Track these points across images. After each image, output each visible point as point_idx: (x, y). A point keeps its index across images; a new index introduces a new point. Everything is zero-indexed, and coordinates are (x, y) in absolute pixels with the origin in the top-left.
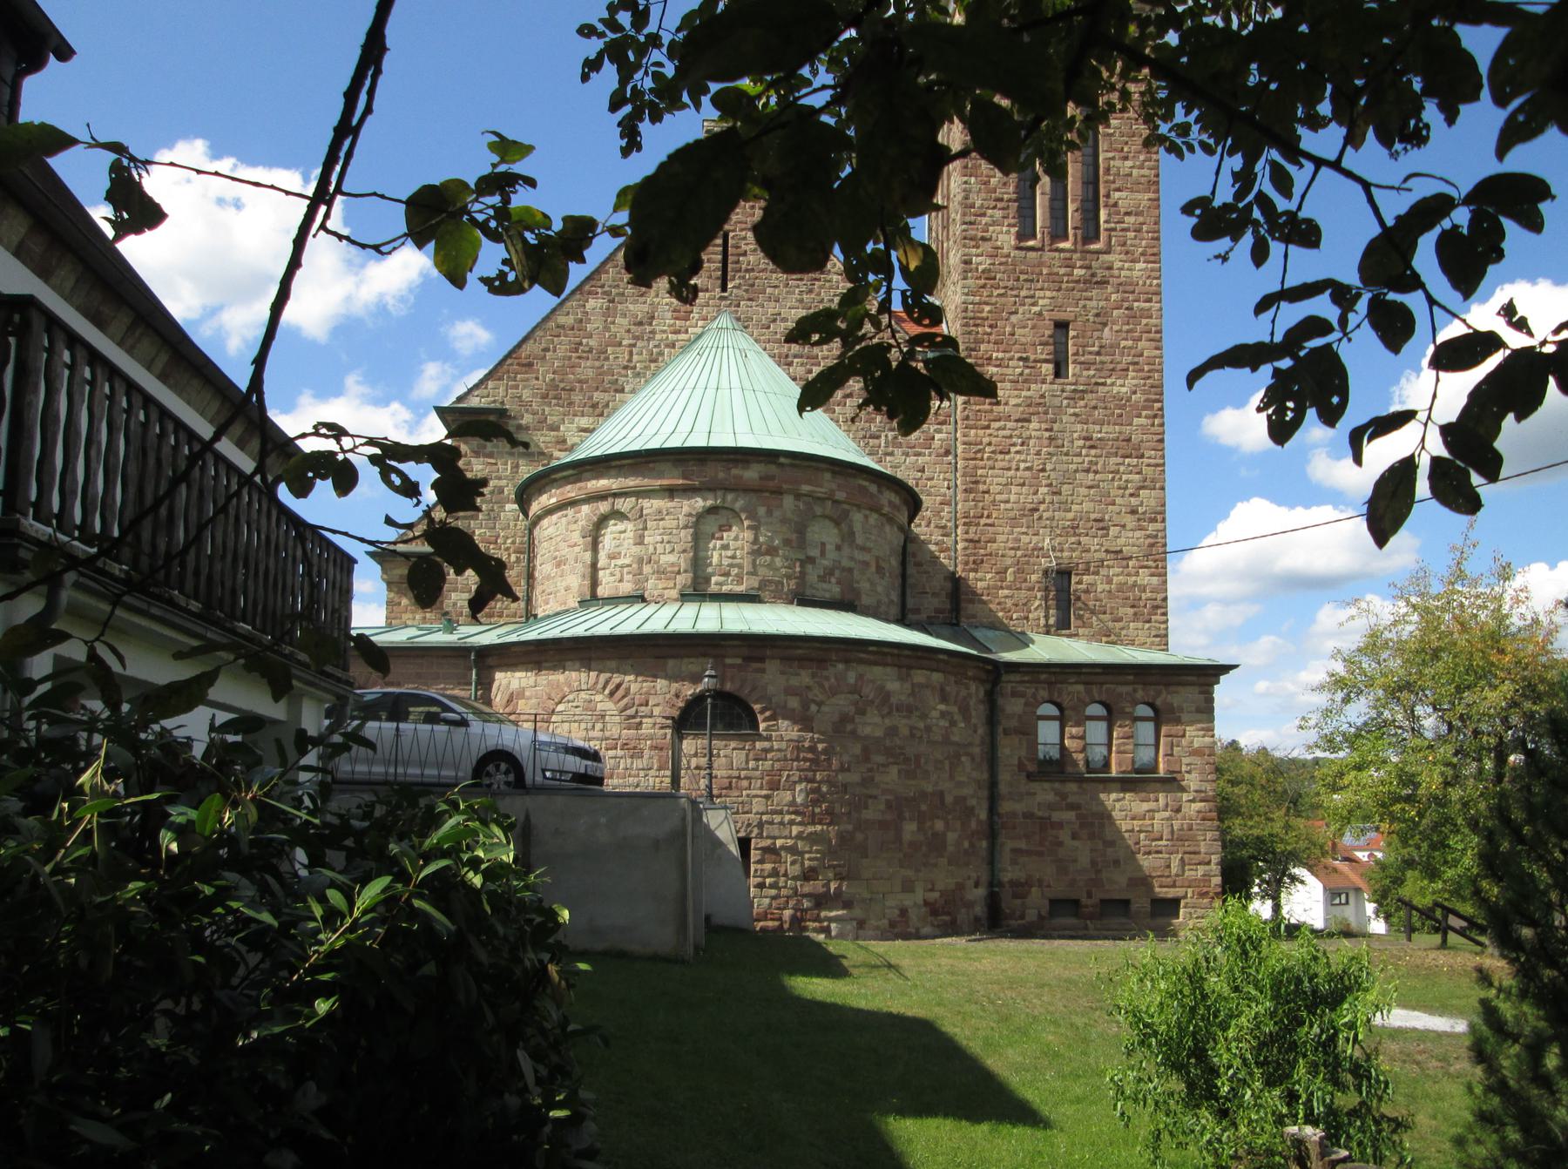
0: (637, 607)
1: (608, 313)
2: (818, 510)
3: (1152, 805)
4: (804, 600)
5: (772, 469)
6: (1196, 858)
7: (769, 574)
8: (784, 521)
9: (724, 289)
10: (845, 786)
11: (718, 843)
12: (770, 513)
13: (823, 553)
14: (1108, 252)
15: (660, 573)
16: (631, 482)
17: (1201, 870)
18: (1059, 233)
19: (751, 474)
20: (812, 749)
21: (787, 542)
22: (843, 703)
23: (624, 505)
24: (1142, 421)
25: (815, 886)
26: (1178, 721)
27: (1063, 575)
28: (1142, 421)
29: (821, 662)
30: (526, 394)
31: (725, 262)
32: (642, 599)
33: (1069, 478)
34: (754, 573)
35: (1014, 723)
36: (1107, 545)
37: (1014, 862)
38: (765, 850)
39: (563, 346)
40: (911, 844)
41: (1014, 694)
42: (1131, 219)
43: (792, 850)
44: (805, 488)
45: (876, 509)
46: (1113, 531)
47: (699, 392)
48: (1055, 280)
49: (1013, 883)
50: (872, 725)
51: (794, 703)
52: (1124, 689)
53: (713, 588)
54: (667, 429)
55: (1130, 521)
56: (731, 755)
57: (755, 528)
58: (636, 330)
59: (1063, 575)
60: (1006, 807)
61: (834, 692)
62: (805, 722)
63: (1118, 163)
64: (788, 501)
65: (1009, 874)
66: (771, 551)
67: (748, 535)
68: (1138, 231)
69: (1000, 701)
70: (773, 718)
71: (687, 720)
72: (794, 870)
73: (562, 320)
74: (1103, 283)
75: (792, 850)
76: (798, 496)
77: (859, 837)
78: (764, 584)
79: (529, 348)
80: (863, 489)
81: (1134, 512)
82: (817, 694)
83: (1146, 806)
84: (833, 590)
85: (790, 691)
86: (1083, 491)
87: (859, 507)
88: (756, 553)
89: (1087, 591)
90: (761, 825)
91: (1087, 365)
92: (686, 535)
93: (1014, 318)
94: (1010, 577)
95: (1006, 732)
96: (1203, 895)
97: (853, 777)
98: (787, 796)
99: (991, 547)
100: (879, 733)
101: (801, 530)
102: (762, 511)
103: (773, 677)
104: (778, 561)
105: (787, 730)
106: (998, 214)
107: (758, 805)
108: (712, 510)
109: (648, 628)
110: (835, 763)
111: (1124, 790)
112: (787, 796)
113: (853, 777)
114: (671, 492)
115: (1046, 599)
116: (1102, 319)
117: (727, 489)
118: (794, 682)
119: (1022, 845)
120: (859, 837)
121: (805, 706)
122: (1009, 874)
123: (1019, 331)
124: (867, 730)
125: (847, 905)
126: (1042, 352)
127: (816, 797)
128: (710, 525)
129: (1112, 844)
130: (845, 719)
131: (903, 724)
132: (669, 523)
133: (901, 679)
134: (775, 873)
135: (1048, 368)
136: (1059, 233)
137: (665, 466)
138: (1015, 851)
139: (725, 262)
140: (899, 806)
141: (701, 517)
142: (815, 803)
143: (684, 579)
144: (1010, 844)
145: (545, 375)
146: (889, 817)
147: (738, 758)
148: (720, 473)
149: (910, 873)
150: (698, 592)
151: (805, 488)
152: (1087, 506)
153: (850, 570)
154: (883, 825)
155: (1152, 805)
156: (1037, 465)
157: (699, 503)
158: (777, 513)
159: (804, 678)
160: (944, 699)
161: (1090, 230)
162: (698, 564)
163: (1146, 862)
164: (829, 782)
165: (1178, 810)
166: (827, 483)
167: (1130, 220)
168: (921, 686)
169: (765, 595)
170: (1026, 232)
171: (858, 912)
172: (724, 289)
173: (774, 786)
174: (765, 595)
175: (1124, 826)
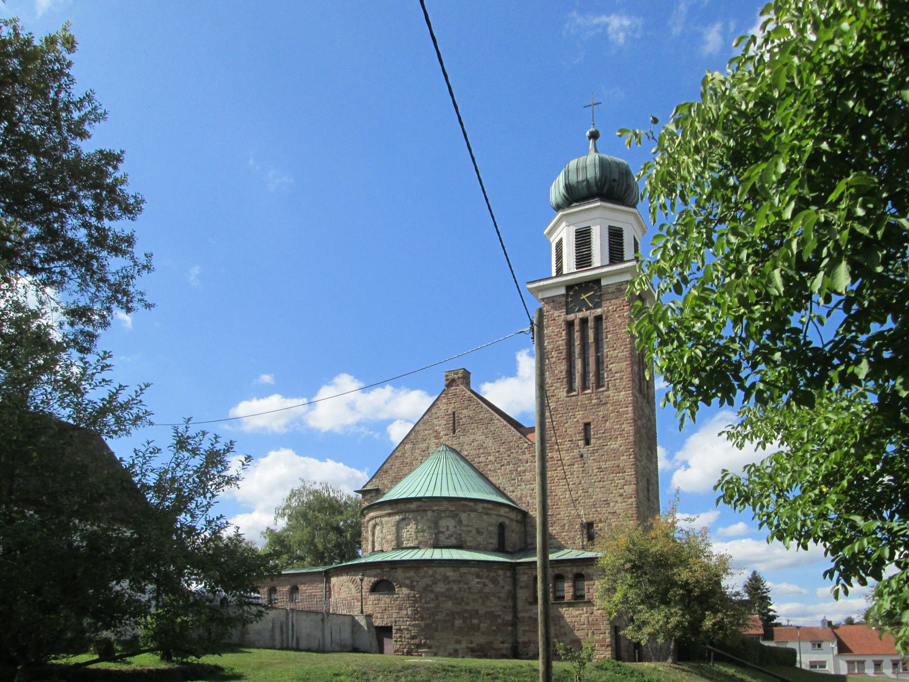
0: (416, 551)
1: (413, 449)
2: (443, 515)
3: (581, 612)
4: (436, 546)
5: (420, 503)
6: (599, 632)
7: (422, 539)
8: (428, 520)
9: (454, 432)
10: (428, 609)
11: (361, 626)
12: (422, 518)
13: (448, 529)
14: (608, 390)
15: (387, 541)
16: (378, 513)
17: (602, 636)
18: (584, 387)
19: (413, 506)
20: (414, 597)
21: (429, 527)
22: (427, 581)
23: (378, 520)
24: (625, 457)
25: (417, 641)
26: (592, 579)
27: (589, 526)
28: (625, 457)
29: (418, 568)
30: (386, 482)
31: (454, 423)
32: (382, 551)
33: (592, 485)
34: (417, 539)
35: (523, 584)
36: (609, 510)
37: (523, 635)
38: (397, 630)
39: (398, 463)
40: (459, 628)
41: (524, 574)
42: (618, 375)
43: (407, 629)
44: (435, 508)
45: (475, 511)
46: (612, 504)
47: (435, 476)
48: (584, 407)
49: (523, 642)
50: (440, 588)
51: (407, 582)
52: (568, 569)
53: (404, 545)
54: (418, 490)
55: (620, 499)
56: (385, 599)
57: (417, 524)
58: (423, 454)
59: (589, 526)
60: (520, 615)
61: (423, 577)
62: (412, 588)
63: (612, 352)
64: (429, 514)
65: (522, 639)
66: (423, 531)
67: (414, 527)
68: (621, 379)
69: (518, 577)
70: (400, 587)
71: (374, 589)
72: (409, 636)
73: (397, 454)
74: (606, 403)
75: (407, 629)
76: (434, 511)
77: (434, 625)
78: (420, 543)
79: (387, 465)
80: (466, 506)
81: (621, 495)
82: (417, 578)
83: (578, 612)
84: (453, 541)
85: (408, 578)
86: (598, 490)
87: (464, 512)
88: (417, 532)
89: (600, 530)
90: (396, 622)
91: (599, 439)
92: (394, 529)
93: (566, 425)
94: (566, 527)
95: (521, 588)
96: (602, 646)
97: (431, 605)
98: (405, 612)
99: (559, 516)
100: (443, 590)
101: (436, 524)
102: (419, 518)
103: (400, 573)
104: (426, 534)
105: (405, 591)
106: (558, 384)
107: (395, 615)
108: (403, 519)
109: (414, 558)
110: (423, 601)
111: (569, 607)
112: (405, 612)
113: (431, 605)
114: (389, 515)
115: (582, 534)
116: (605, 418)
117: (406, 512)
118: (408, 575)
119: (527, 628)
120: (434, 625)
121: (412, 582)
122: (522, 639)
123: (568, 430)
124: (438, 589)
125: (429, 647)
126: (579, 437)
127: (416, 612)
128: (403, 524)
129: (563, 627)
130: (427, 586)
131: (455, 587)
132: (389, 525)
133: (454, 571)
134: (401, 637)
135: (581, 443)
136: (584, 387)
137: (386, 507)
138: (525, 631)
139: (454, 423)
140: (452, 615)
141: (398, 522)
142: (415, 614)
143: (394, 543)
144: (522, 628)
145: (392, 474)
146: (447, 618)
147: (388, 600)
148: (402, 506)
149: (460, 638)
150: (399, 547)
151: (435, 508)
152: (600, 495)
153: (460, 534)
154: (445, 621)
155: (581, 612)
156: (577, 481)
157: (397, 518)
158: (425, 518)
159: (412, 573)
160: (478, 576)
161: (599, 383)
162: (398, 538)
163: (577, 633)
164: (420, 607)
165: (592, 613)
166: (445, 504)
167: (617, 375)
168: (464, 573)
169: (421, 546)
170: (570, 389)
171: (434, 650)
172: (454, 432)
173: (401, 609)
174: (421, 546)
175: (568, 620)
